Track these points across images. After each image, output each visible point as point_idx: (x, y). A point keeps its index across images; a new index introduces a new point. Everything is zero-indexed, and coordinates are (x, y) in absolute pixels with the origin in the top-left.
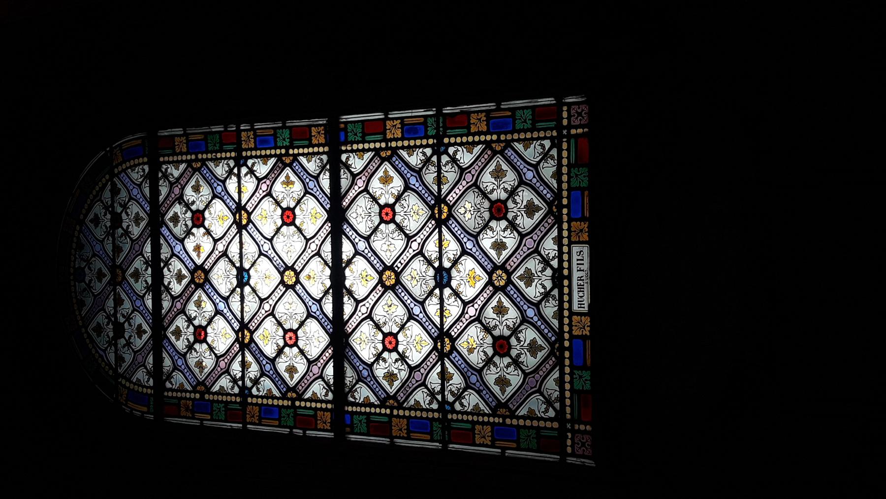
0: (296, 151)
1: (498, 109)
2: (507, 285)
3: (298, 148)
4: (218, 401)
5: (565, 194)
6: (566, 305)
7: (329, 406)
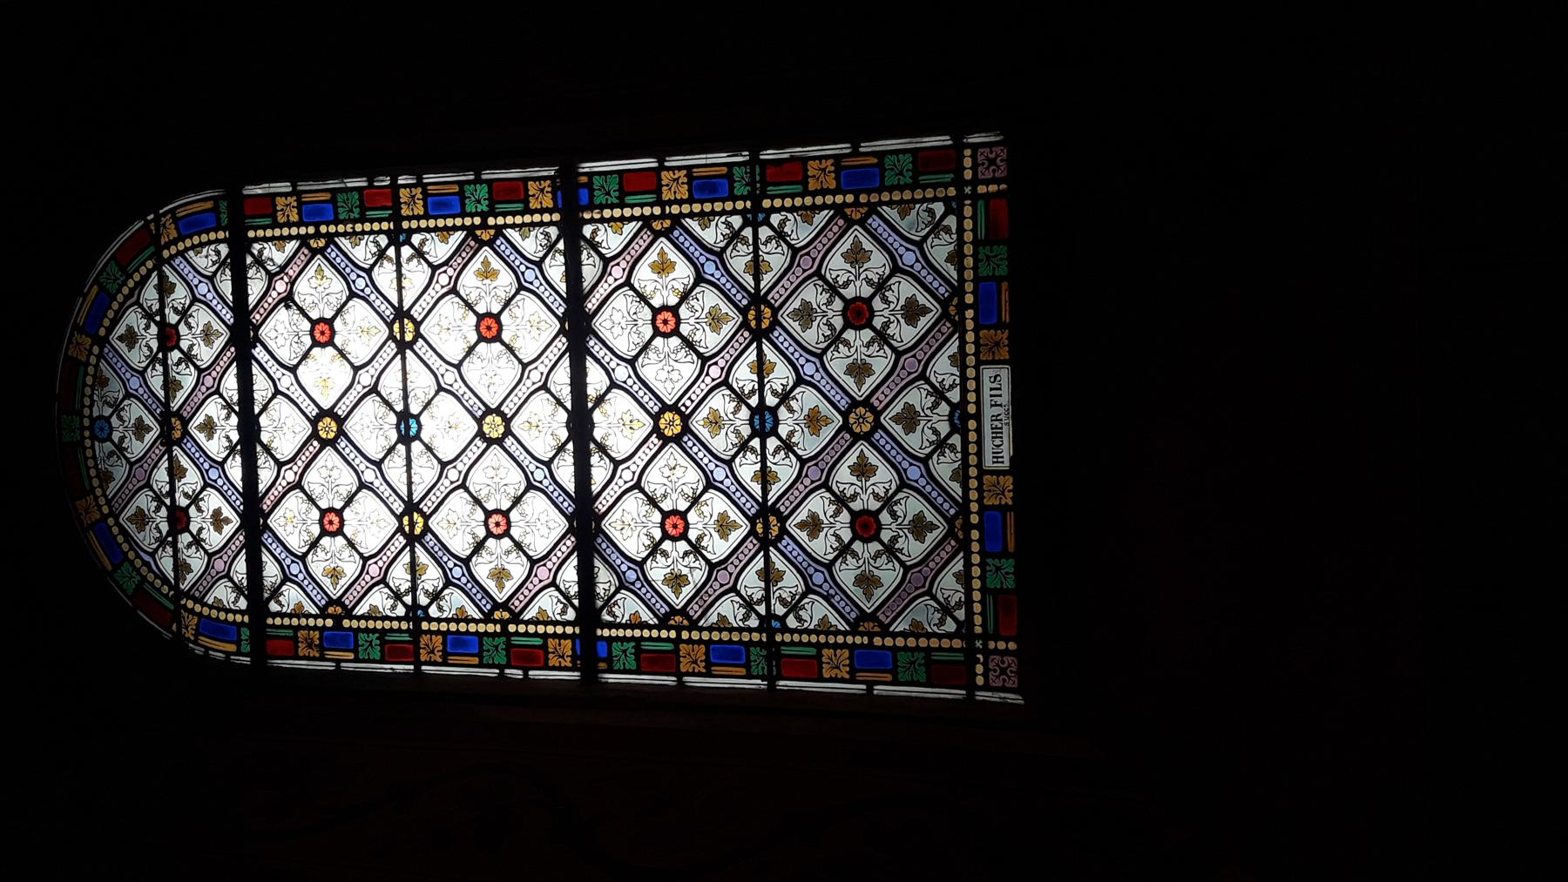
0: (500, 221)
3: (504, 215)
4: (367, 630)
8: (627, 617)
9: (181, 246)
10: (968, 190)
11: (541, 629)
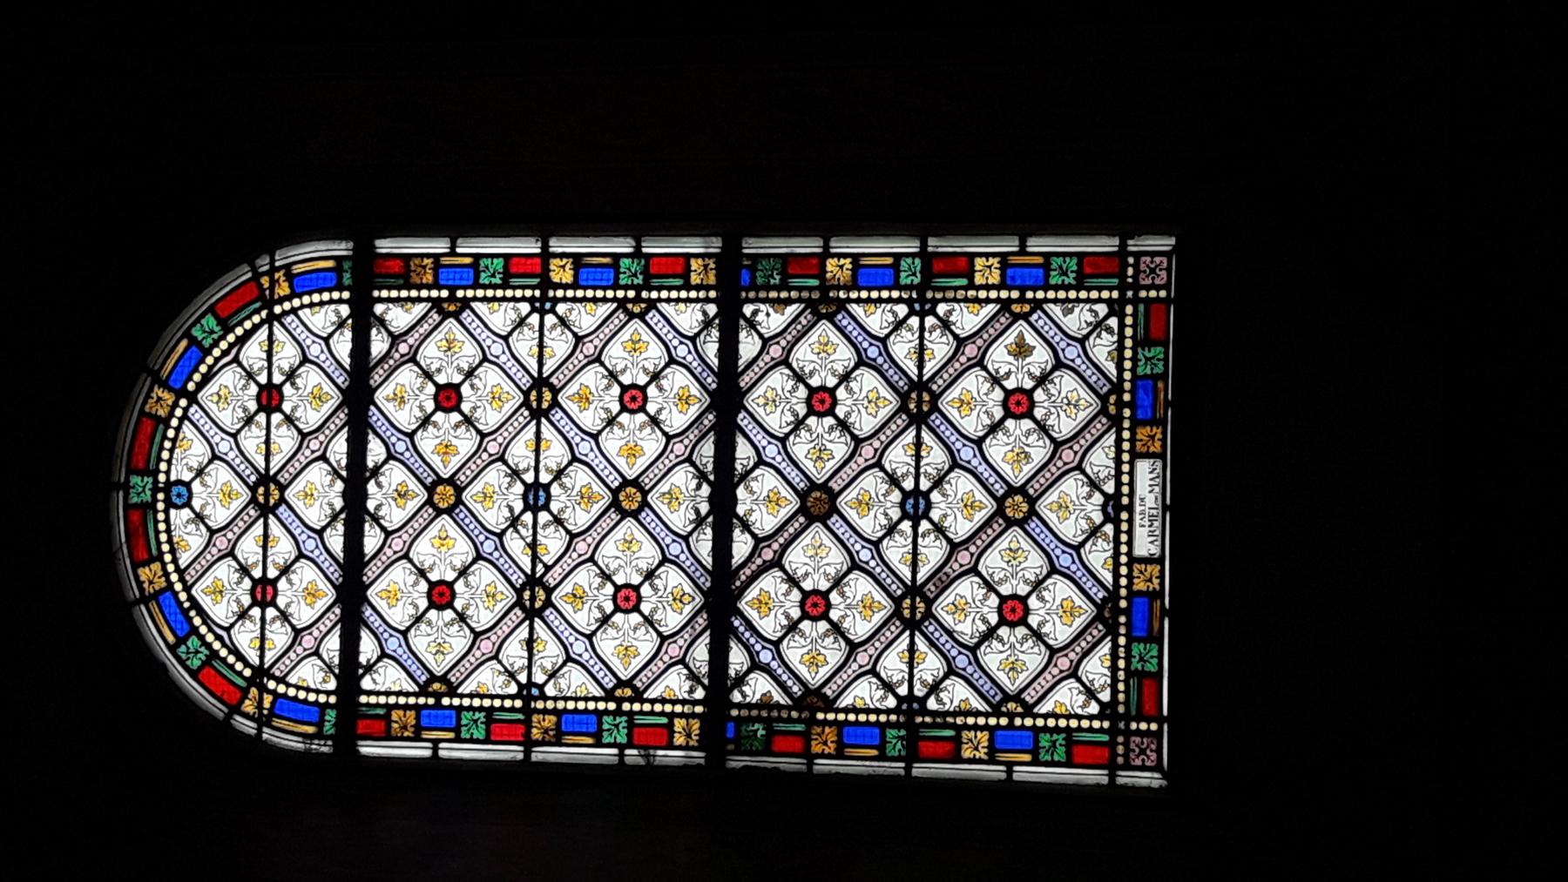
0: (654, 295)
1: (453, 253)
2: (1006, 518)
3: (659, 289)
4: (471, 708)
5: (1127, 386)
6: (1124, 549)
7: (699, 709)
8: (758, 696)
9: (296, 302)
10: (1130, 294)
11: (668, 708)
